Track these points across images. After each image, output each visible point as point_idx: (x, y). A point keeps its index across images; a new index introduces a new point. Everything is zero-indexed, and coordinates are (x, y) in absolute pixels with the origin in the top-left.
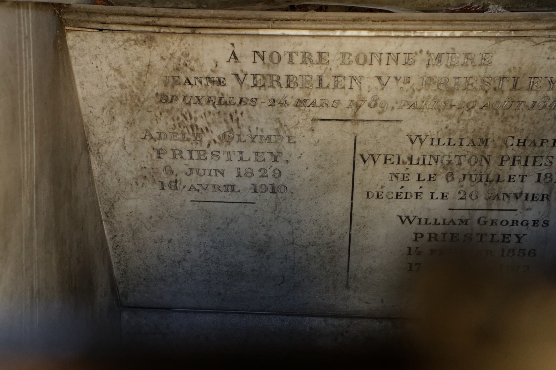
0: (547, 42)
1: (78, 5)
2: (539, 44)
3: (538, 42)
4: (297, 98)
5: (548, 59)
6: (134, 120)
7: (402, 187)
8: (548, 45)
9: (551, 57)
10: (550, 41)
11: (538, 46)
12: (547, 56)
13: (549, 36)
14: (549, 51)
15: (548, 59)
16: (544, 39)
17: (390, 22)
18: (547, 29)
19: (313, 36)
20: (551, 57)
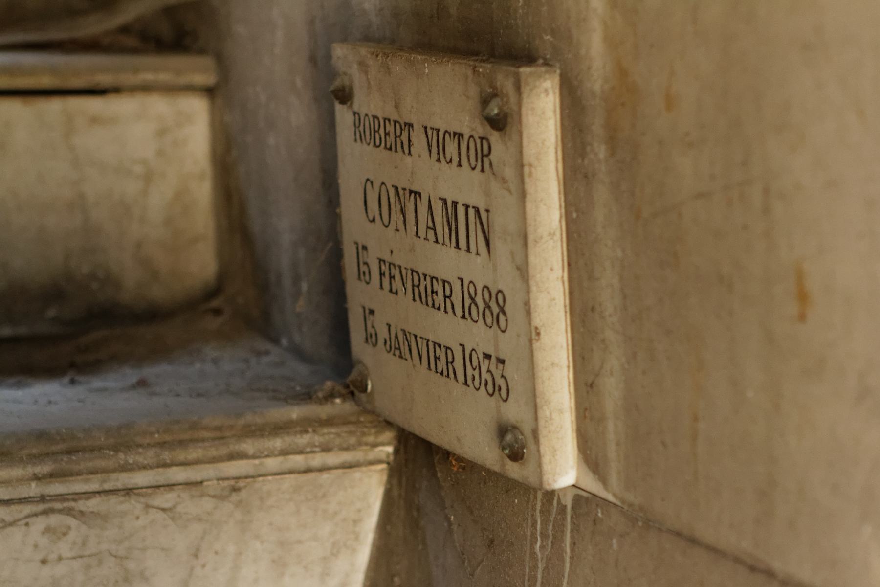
0: (36, 515)
1: (124, 507)
2: (12, 524)
3: (8, 518)
4: (345, 106)
5: (44, 562)
6: (336, 513)
7: (420, 156)
8: (40, 523)
9: (53, 556)
10: (45, 512)
11: (9, 530)
12: (40, 556)
13: (43, 499)
14: (44, 541)
15: (44, 562)
16: (27, 509)
17: (79, 478)
18: (37, 478)
19: (464, 358)
20: (53, 556)
